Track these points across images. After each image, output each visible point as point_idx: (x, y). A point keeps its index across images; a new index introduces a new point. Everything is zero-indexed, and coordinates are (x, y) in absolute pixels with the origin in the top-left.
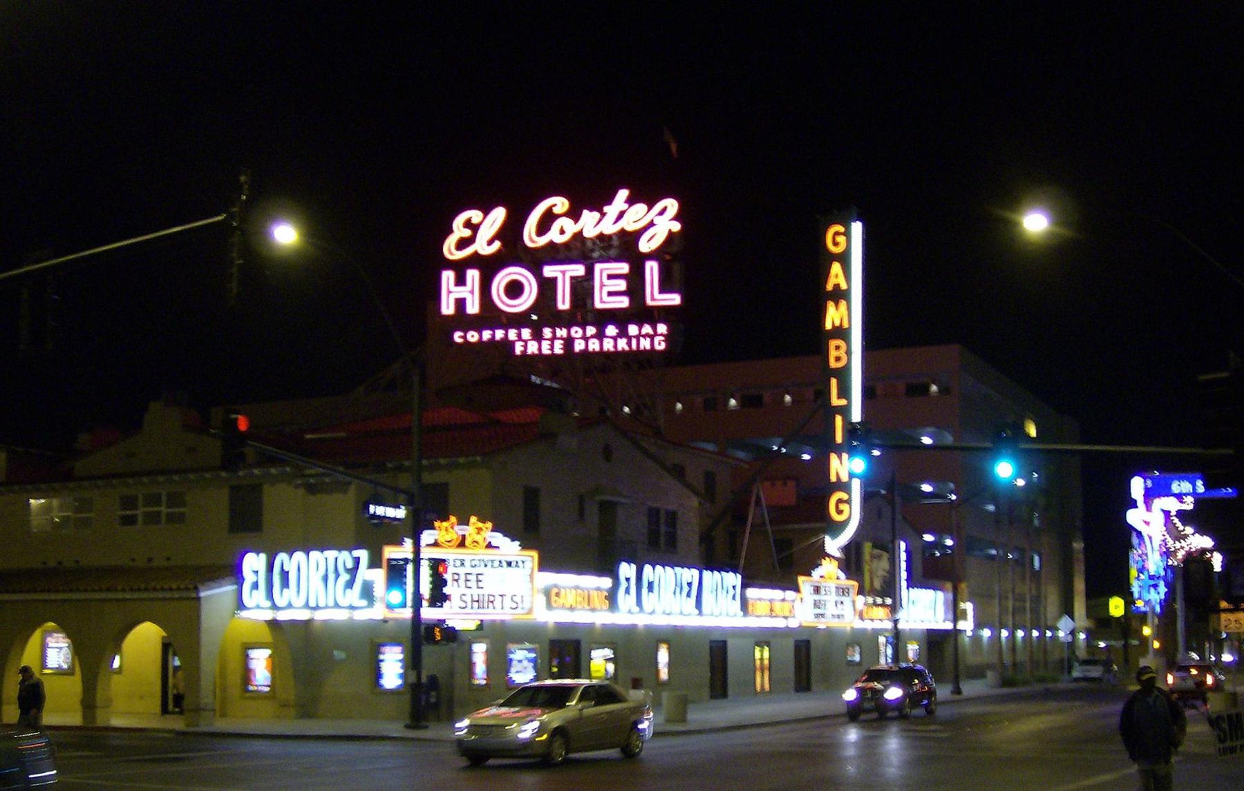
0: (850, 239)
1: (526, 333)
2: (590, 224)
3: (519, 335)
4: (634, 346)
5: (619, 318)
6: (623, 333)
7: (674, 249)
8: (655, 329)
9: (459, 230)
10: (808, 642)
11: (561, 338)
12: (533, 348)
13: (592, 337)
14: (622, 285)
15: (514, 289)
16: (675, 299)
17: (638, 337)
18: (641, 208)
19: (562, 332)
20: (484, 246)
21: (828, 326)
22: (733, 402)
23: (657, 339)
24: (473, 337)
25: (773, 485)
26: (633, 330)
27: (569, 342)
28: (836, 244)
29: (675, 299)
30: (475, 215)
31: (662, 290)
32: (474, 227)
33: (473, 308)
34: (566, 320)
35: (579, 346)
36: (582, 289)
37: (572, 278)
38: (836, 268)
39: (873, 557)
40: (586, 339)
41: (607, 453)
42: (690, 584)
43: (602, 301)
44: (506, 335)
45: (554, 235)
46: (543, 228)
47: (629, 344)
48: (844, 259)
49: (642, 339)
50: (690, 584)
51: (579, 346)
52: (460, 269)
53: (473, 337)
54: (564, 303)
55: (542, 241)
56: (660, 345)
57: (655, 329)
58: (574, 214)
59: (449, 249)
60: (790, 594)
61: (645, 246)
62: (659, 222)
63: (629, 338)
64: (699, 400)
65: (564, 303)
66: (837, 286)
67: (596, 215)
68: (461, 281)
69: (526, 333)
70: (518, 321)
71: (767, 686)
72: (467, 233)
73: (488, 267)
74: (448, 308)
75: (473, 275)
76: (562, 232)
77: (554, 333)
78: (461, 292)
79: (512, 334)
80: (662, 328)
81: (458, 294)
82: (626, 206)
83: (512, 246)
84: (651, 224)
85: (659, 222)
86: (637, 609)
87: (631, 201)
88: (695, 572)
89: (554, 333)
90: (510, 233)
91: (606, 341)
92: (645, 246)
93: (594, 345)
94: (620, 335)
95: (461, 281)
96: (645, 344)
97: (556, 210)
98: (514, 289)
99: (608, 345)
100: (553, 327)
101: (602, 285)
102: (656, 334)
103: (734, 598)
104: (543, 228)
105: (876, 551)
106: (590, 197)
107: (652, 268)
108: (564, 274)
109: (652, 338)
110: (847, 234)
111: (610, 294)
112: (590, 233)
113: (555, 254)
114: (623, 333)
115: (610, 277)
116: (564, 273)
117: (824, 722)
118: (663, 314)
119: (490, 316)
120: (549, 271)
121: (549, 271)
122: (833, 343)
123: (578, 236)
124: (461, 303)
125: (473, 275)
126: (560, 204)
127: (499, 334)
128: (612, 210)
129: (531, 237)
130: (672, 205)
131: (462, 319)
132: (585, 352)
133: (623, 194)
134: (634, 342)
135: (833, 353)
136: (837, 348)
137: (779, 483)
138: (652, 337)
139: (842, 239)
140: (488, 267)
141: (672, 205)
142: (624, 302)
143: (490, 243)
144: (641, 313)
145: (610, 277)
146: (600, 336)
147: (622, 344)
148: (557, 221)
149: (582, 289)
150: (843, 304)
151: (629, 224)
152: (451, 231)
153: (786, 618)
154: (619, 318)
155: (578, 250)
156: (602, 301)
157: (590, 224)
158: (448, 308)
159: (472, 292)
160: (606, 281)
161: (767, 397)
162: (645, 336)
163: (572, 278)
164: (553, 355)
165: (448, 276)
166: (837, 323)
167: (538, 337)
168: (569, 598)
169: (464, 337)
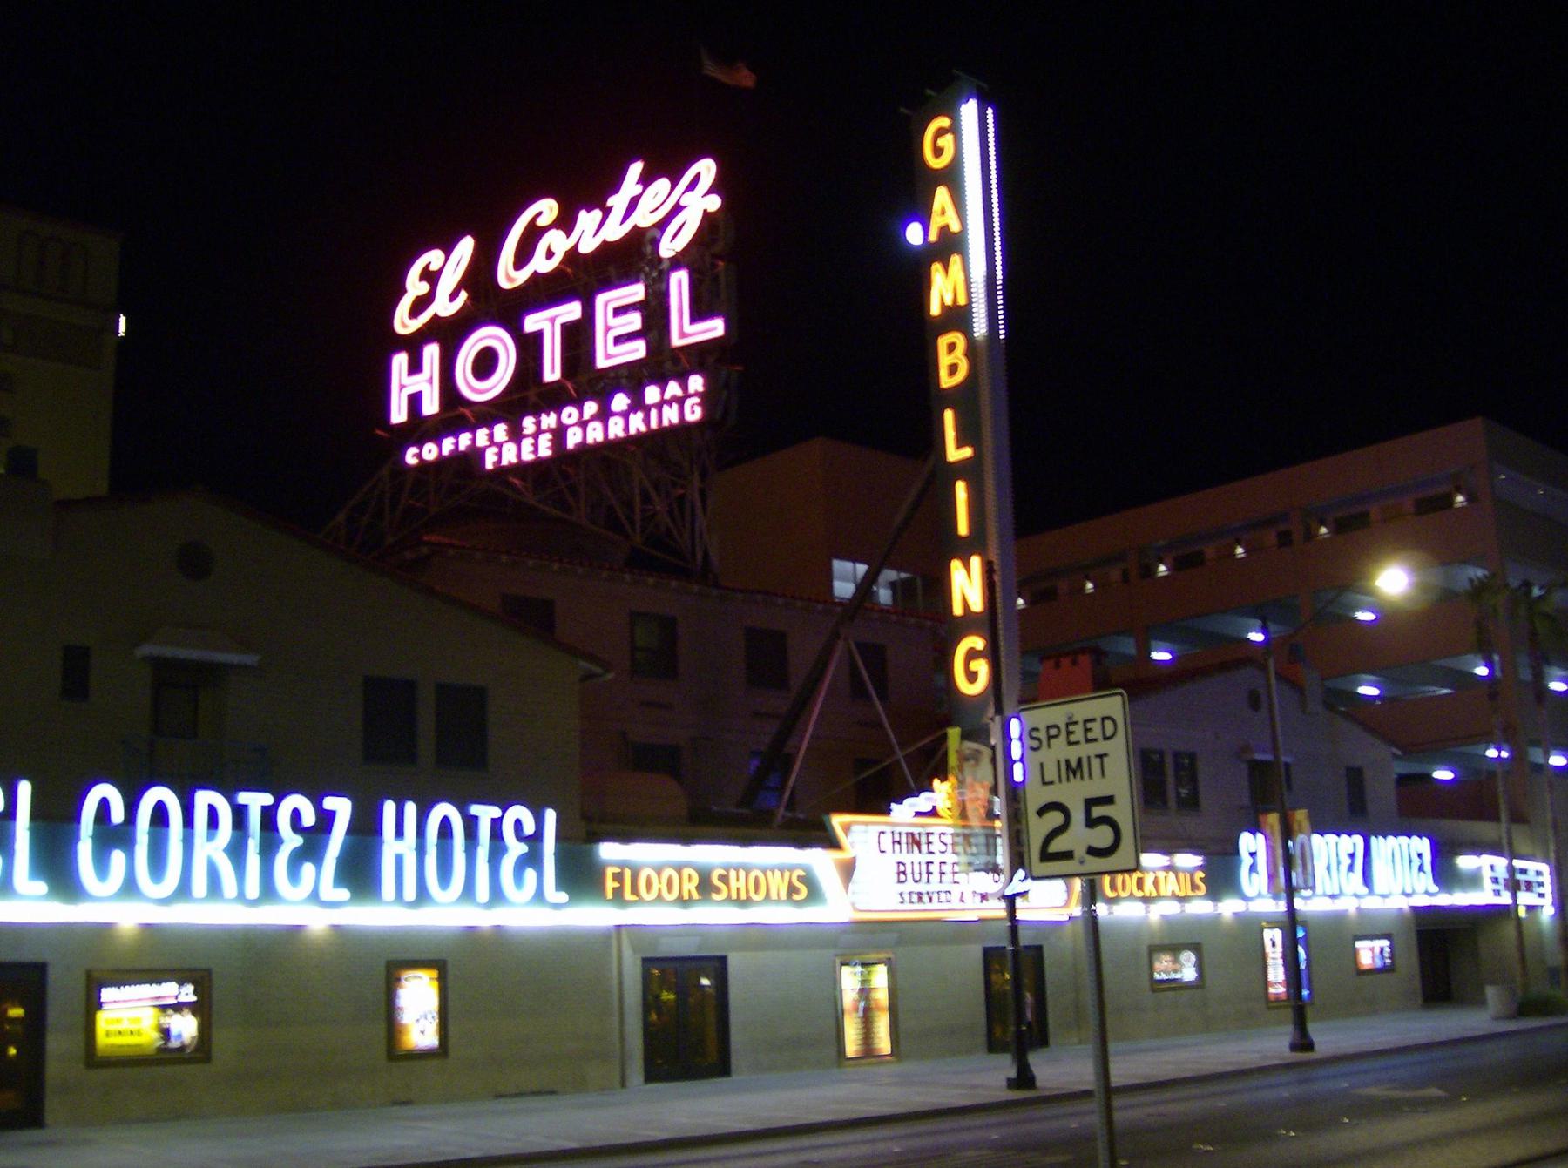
0: (963, 138)
1: (500, 431)
2: (591, 231)
3: (491, 436)
4: (654, 424)
5: (632, 379)
6: (638, 404)
7: (718, 248)
8: (685, 387)
9: (415, 286)
10: (1039, 948)
11: (550, 430)
12: (509, 455)
13: (593, 418)
14: (634, 321)
15: (485, 363)
16: (715, 328)
17: (659, 406)
18: (663, 184)
19: (549, 421)
20: (444, 307)
21: (935, 310)
22: (1162, 568)
23: (688, 403)
24: (430, 452)
25: (1057, 665)
26: (652, 394)
27: (560, 433)
28: (938, 152)
29: (715, 328)
30: (434, 258)
31: (694, 319)
32: (431, 277)
33: (431, 406)
34: (554, 399)
35: (573, 438)
36: (578, 338)
37: (564, 326)
38: (942, 196)
39: (964, 758)
40: (583, 424)
41: (194, 562)
42: (1352, 856)
43: (608, 355)
44: (474, 440)
45: (541, 264)
46: (523, 256)
47: (647, 420)
48: (952, 177)
49: (666, 408)
50: (1352, 856)
51: (573, 438)
52: (413, 345)
53: (430, 452)
54: (552, 372)
55: (522, 276)
56: (694, 413)
57: (685, 387)
58: (566, 222)
59: (404, 323)
60: (817, 859)
61: (669, 248)
62: (678, 204)
63: (647, 410)
64: (1115, 574)
65: (552, 372)
66: (944, 230)
67: (597, 214)
68: (415, 367)
69: (500, 431)
70: (488, 414)
71: (883, 1043)
72: (424, 288)
73: (449, 333)
74: (399, 414)
75: (432, 352)
76: (550, 254)
77: (538, 424)
78: (417, 383)
79: (482, 436)
80: (696, 383)
81: (411, 386)
82: (639, 188)
83: (487, 301)
84: (678, 209)
85: (678, 204)
86: (1365, 890)
87: (646, 180)
88: (1358, 840)
89: (538, 424)
90: (479, 277)
91: (612, 421)
92: (669, 248)
93: (595, 434)
94: (633, 408)
95: (415, 367)
96: (671, 415)
97: (542, 222)
98: (485, 363)
99: (616, 428)
100: (537, 415)
101: (608, 329)
102: (687, 396)
103: (1421, 869)
104: (523, 256)
105: (971, 746)
106: (586, 189)
107: (679, 281)
108: (546, 323)
109: (679, 404)
110: (955, 129)
111: (618, 340)
112: (587, 247)
113: (544, 292)
114: (638, 404)
115: (618, 312)
116: (552, 320)
117: (1167, 1095)
118: (699, 357)
119: (458, 412)
120: (532, 323)
121: (532, 323)
122: (943, 342)
123: (573, 255)
124: (415, 400)
125: (432, 352)
126: (547, 209)
127: (465, 440)
128: (618, 202)
129: (509, 276)
130: (706, 169)
131: (420, 428)
132: (583, 447)
133: (636, 169)
134: (654, 413)
135: (945, 360)
136: (952, 347)
137: (1065, 662)
138: (681, 401)
139: (947, 142)
140: (449, 333)
141: (706, 169)
142: (638, 350)
143: (453, 297)
144: (664, 363)
145: (618, 312)
146: (604, 415)
147: (637, 423)
148: (549, 235)
149: (578, 338)
150: (955, 260)
151: (644, 218)
152: (403, 291)
153: (1333, 896)
154: (632, 379)
155: (582, 277)
156: (608, 355)
157: (591, 231)
158: (399, 414)
159: (430, 381)
160: (612, 321)
161: (1210, 551)
162: (669, 403)
163: (564, 326)
164: (539, 462)
165: (400, 361)
166: (949, 302)
167: (516, 435)
168: (778, 885)
169: (419, 456)
